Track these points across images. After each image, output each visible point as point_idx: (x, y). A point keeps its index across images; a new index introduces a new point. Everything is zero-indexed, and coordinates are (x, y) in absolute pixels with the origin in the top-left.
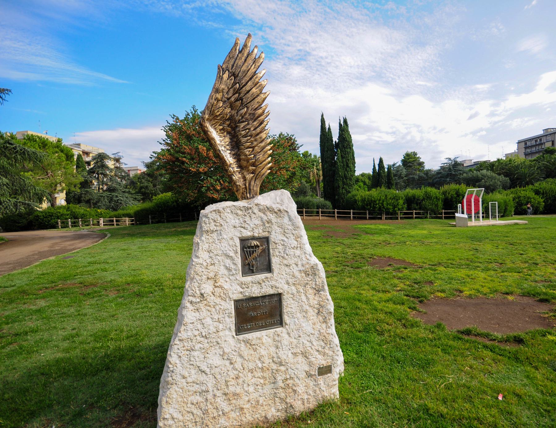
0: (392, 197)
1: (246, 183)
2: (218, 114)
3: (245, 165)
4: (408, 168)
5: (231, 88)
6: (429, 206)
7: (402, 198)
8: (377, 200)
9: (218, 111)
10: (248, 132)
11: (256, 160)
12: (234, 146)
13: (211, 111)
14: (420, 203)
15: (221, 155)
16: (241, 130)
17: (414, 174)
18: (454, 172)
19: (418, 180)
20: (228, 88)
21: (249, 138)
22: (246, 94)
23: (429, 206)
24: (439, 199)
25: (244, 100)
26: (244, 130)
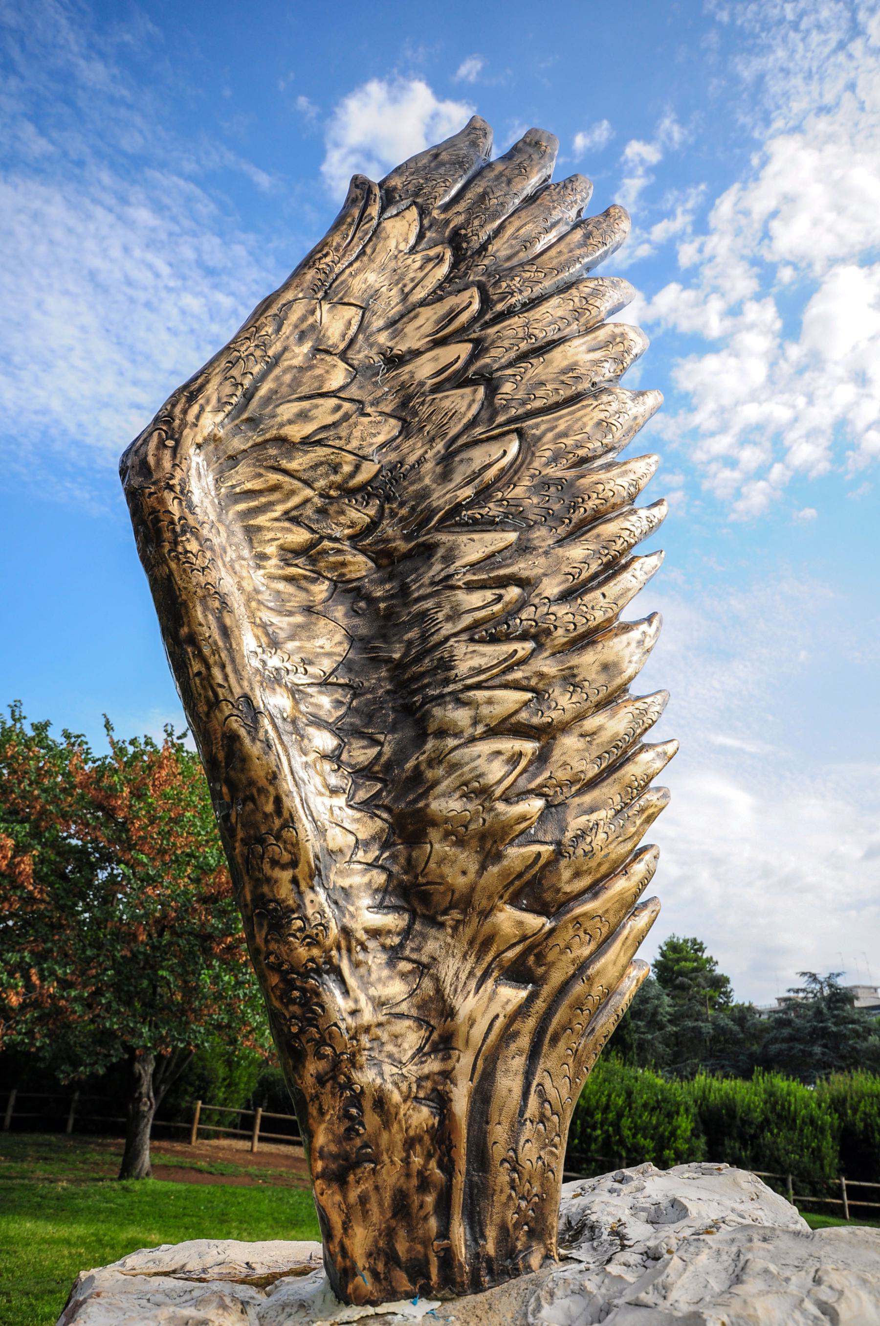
0: (652, 1103)
1: (447, 1075)
2: (296, 432)
3: (461, 882)
4: (676, 992)
5: (423, 303)
6: (788, 1153)
7: (687, 1110)
8: (597, 1107)
9: (303, 416)
10: (522, 604)
11: (559, 853)
12: (379, 704)
13: (249, 396)
14: (754, 1137)
15: (254, 749)
16: (459, 580)
17: (699, 1017)
18: (835, 1024)
19: (714, 1039)
20: (405, 296)
21: (524, 648)
22: (524, 357)
23: (788, 1153)
24: (822, 1130)
25: (507, 388)
26: (483, 586)
